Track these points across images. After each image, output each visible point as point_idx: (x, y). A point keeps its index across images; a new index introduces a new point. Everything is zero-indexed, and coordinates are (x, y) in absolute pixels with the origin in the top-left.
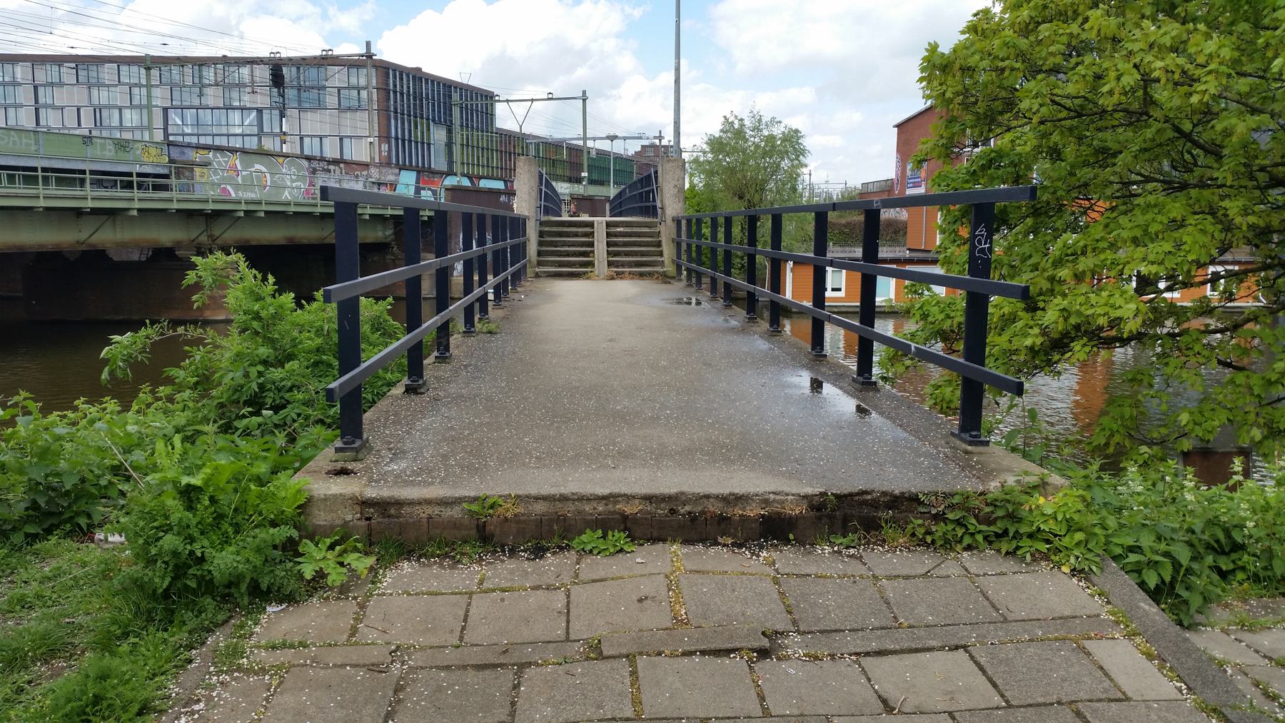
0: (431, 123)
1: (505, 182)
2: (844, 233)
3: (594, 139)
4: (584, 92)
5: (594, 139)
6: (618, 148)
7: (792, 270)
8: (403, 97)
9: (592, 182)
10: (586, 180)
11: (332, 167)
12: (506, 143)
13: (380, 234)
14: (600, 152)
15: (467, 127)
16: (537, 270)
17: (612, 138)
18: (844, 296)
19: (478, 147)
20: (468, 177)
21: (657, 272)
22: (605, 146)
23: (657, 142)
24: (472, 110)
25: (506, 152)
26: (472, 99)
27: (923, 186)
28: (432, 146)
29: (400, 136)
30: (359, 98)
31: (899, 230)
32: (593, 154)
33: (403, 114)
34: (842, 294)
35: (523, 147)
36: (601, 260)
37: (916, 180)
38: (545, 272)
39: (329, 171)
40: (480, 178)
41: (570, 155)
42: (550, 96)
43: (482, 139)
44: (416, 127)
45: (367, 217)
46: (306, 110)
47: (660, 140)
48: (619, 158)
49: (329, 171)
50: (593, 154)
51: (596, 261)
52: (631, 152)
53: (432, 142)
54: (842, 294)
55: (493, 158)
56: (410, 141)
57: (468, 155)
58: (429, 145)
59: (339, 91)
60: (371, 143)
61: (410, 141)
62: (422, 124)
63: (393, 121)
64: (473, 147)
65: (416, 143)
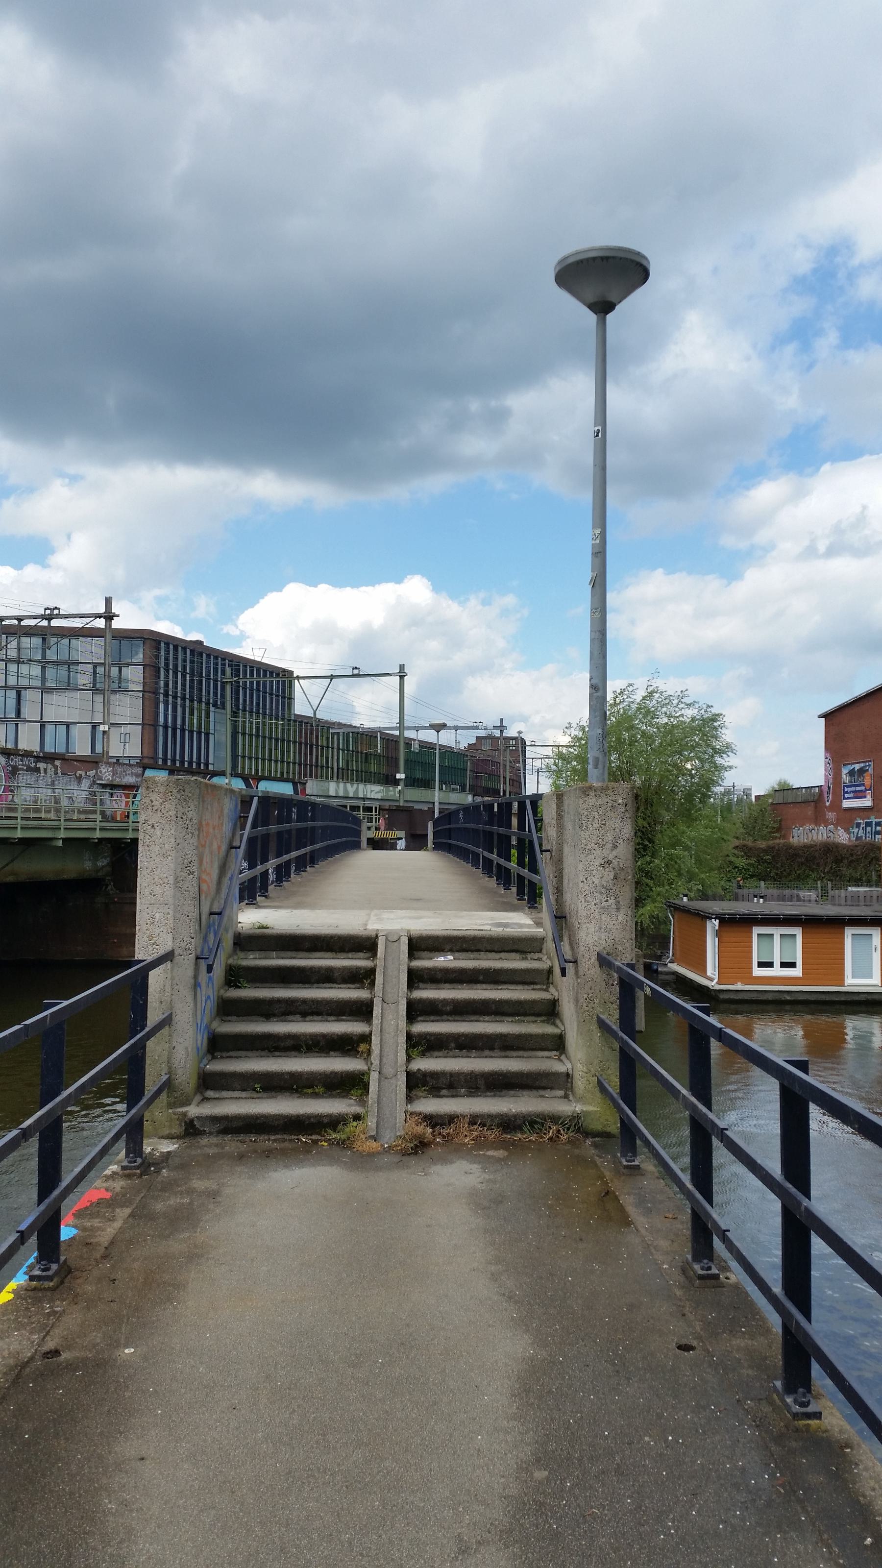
0: (212, 709)
1: (295, 785)
2: (765, 861)
3: (417, 729)
4: (402, 667)
5: (417, 729)
6: (446, 739)
7: (718, 934)
8: (177, 677)
9: (411, 782)
10: (402, 783)
11: (42, 765)
12: (306, 734)
13: (88, 865)
14: (424, 745)
15: (258, 712)
16: (193, 1111)
17: (439, 727)
18: (801, 975)
19: (270, 738)
20: (243, 778)
21: (555, 1119)
22: (429, 736)
23: (497, 733)
24: (252, 690)
25: (306, 744)
26: (252, 675)
27: (869, 797)
28: (211, 737)
29: (170, 725)
30: (120, 678)
31: (843, 858)
32: (415, 747)
33: (175, 697)
34: (797, 972)
35: (328, 738)
36: (388, 1070)
37: (858, 788)
38: (214, 1119)
39: (37, 770)
40: (259, 779)
41: (387, 748)
42: (356, 672)
43: (277, 728)
44: (192, 713)
45: (60, 843)
46: (50, 690)
47: (502, 731)
48: (447, 752)
49: (37, 770)
50: (415, 747)
51: (374, 1077)
52: (463, 746)
53: (211, 731)
54: (797, 972)
55: (289, 751)
56: (183, 730)
57: (257, 747)
58: (207, 735)
59: (95, 667)
60: (104, 732)
61: (183, 730)
62: (200, 710)
63: (162, 706)
64: (264, 737)
65: (191, 732)
